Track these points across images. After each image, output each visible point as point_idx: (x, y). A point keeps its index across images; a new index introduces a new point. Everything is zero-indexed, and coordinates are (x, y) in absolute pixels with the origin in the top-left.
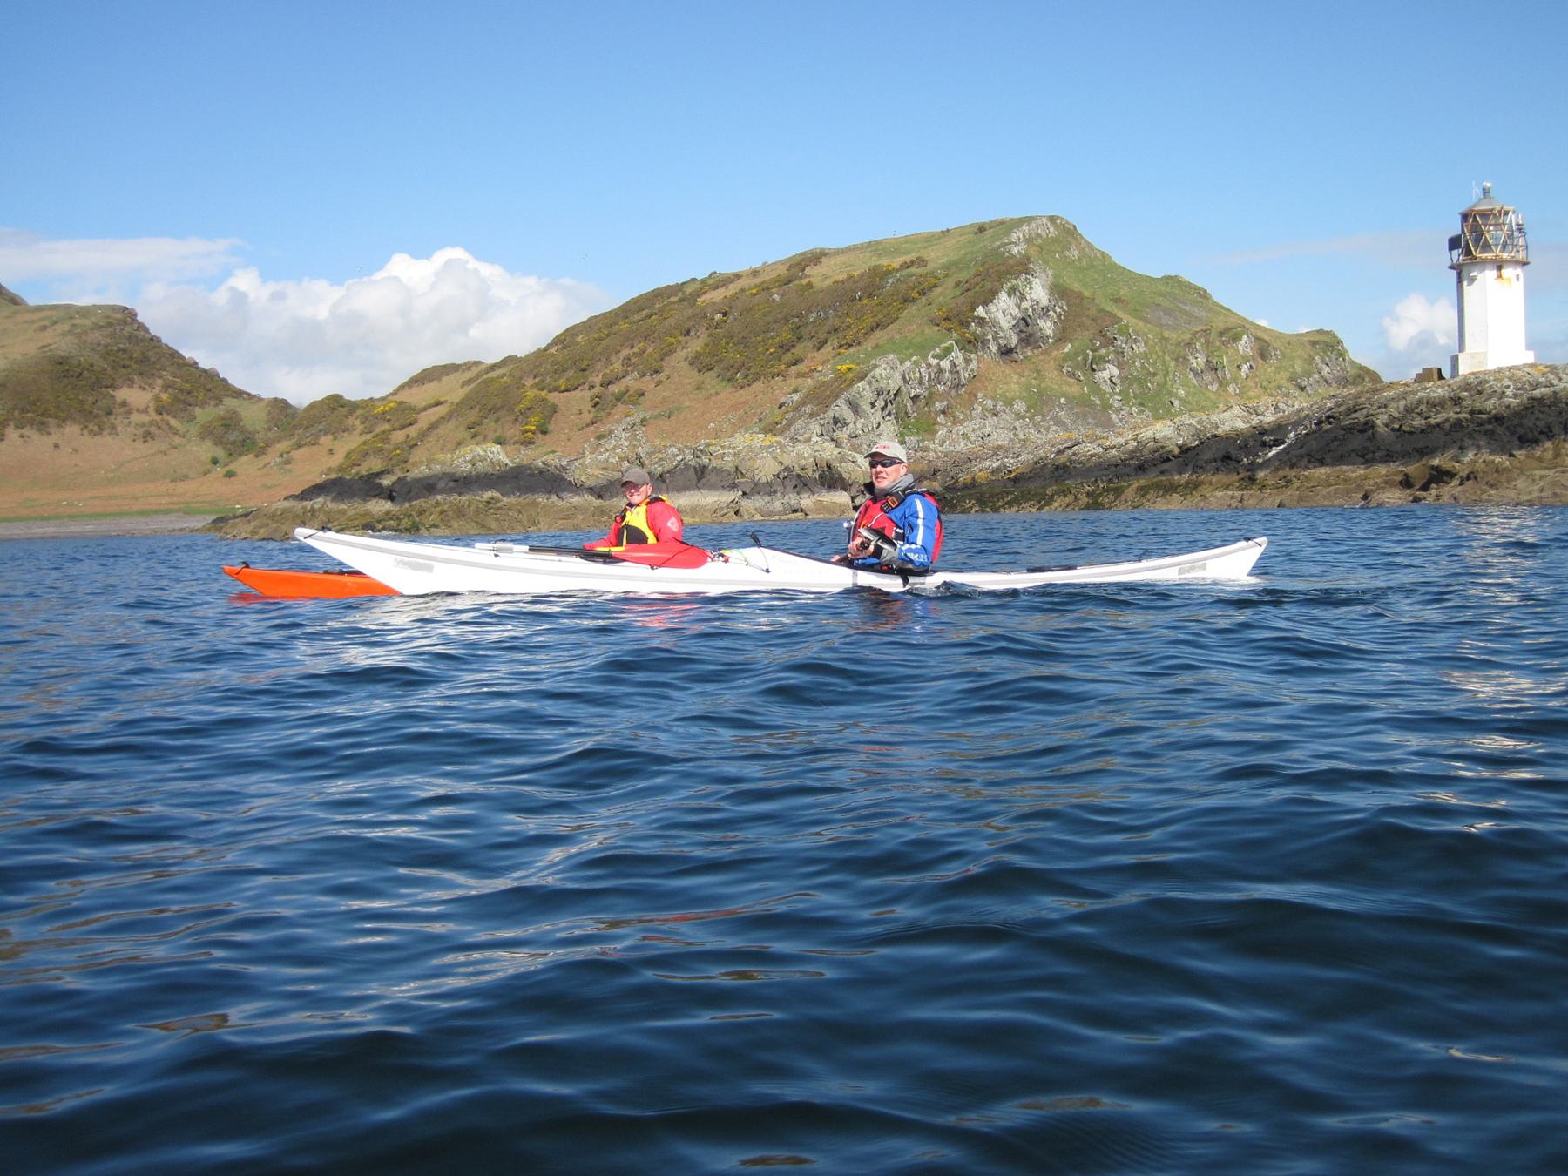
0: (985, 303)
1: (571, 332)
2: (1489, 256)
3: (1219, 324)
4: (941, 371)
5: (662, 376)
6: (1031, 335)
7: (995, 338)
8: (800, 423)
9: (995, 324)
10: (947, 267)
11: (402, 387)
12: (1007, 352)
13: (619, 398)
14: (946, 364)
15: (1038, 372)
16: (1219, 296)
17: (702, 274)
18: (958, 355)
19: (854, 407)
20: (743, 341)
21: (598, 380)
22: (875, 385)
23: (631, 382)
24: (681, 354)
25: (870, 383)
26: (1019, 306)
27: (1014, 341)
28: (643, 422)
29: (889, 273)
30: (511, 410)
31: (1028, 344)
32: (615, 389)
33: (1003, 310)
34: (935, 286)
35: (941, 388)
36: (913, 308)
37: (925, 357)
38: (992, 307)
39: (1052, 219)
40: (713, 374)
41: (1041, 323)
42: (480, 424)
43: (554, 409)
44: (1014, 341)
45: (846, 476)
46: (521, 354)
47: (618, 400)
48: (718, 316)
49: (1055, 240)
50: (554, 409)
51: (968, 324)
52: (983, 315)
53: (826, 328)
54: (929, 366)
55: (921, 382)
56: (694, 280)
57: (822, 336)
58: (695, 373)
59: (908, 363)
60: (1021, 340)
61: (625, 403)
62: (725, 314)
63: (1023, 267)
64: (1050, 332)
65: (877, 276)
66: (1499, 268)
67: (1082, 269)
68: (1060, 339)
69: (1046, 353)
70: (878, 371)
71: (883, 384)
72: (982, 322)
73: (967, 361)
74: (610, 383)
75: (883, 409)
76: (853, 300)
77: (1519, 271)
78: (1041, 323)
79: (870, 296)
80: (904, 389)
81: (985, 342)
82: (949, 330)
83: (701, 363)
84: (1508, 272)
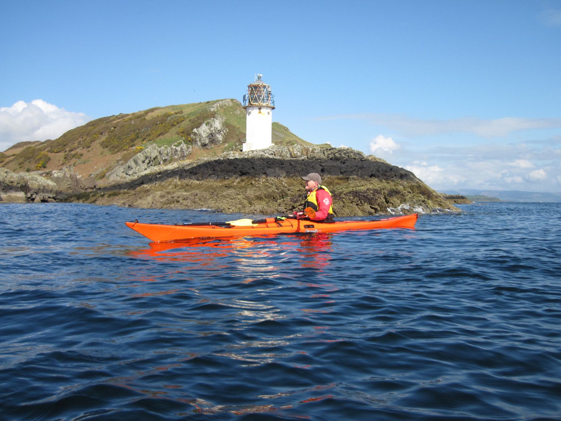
0: (197, 128)
1: (70, 132)
2: (257, 104)
3: (287, 139)
4: (176, 151)
5: (90, 149)
6: (214, 140)
7: (200, 140)
8: (117, 167)
9: (200, 135)
10: (189, 115)
11: (9, 149)
12: (204, 145)
13: (74, 156)
14: (179, 149)
15: (215, 153)
16: (293, 130)
17: (117, 114)
18: (184, 146)
19: (136, 162)
20: (119, 138)
21: (68, 149)
22: (145, 155)
23: (79, 151)
24: (98, 141)
25: (143, 154)
26: (210, 129)
27: (207, 142)
28: (74, 165)
29: (169, 116)
30: (35, 159)
31: (213, 143)
32: (73, 153)
33: (203, 130)
34: (183, 121)
35: (176, 157)
36: (174, 128)
37: (170, 146)
38: (199, 129)
39: (232, 100)
40: (108, 149)
41: (218, 136)
42: (23, 163)
43: (49, 159)
44: (207, 142)
45: (30, 186)
46: (53, 138)
47: (73, 157)
48: (112, 128)
49: (231, 107)
50: (49, 159)
51: (190, 135)
52: (196, 132)
53: (146, 134)
54: (172, 149)
55: (167, 155)
56: (114, 116)
57: (144, 137)
58: (102, 148)
59: (163, 148)
60: (210, 142)
61: (76, 158)
62: (115, 128)
63: (213, 115)
64: (221, 139)
65: (167, 115)
66: (260, 109)
67: (240, 118)
68: (225, 142)
69: (219, 146)
70: (147, 150)
71: (148, 154)
72: (195, 134)
73: (188, 148)
74: (72, 150)
75: (148, 164)
76: (157, 124)
77: (269, 110)
78: (218, 136)
79: (162, 123)
80: (159, 157)
81: (196, 141)
82: (182, 136)
83: (104, 145)
84: (264, 111)
